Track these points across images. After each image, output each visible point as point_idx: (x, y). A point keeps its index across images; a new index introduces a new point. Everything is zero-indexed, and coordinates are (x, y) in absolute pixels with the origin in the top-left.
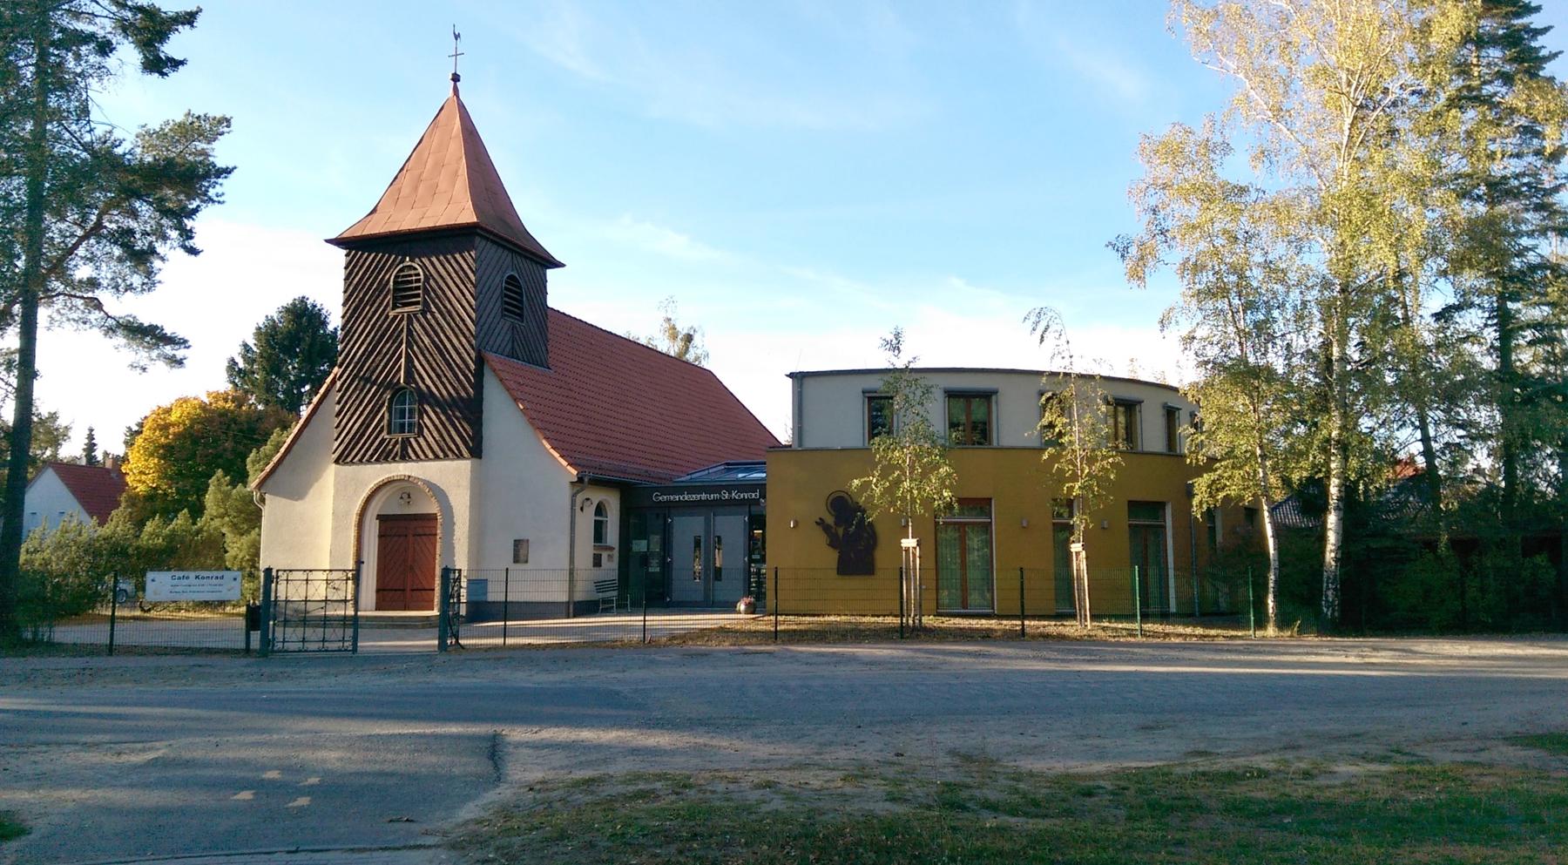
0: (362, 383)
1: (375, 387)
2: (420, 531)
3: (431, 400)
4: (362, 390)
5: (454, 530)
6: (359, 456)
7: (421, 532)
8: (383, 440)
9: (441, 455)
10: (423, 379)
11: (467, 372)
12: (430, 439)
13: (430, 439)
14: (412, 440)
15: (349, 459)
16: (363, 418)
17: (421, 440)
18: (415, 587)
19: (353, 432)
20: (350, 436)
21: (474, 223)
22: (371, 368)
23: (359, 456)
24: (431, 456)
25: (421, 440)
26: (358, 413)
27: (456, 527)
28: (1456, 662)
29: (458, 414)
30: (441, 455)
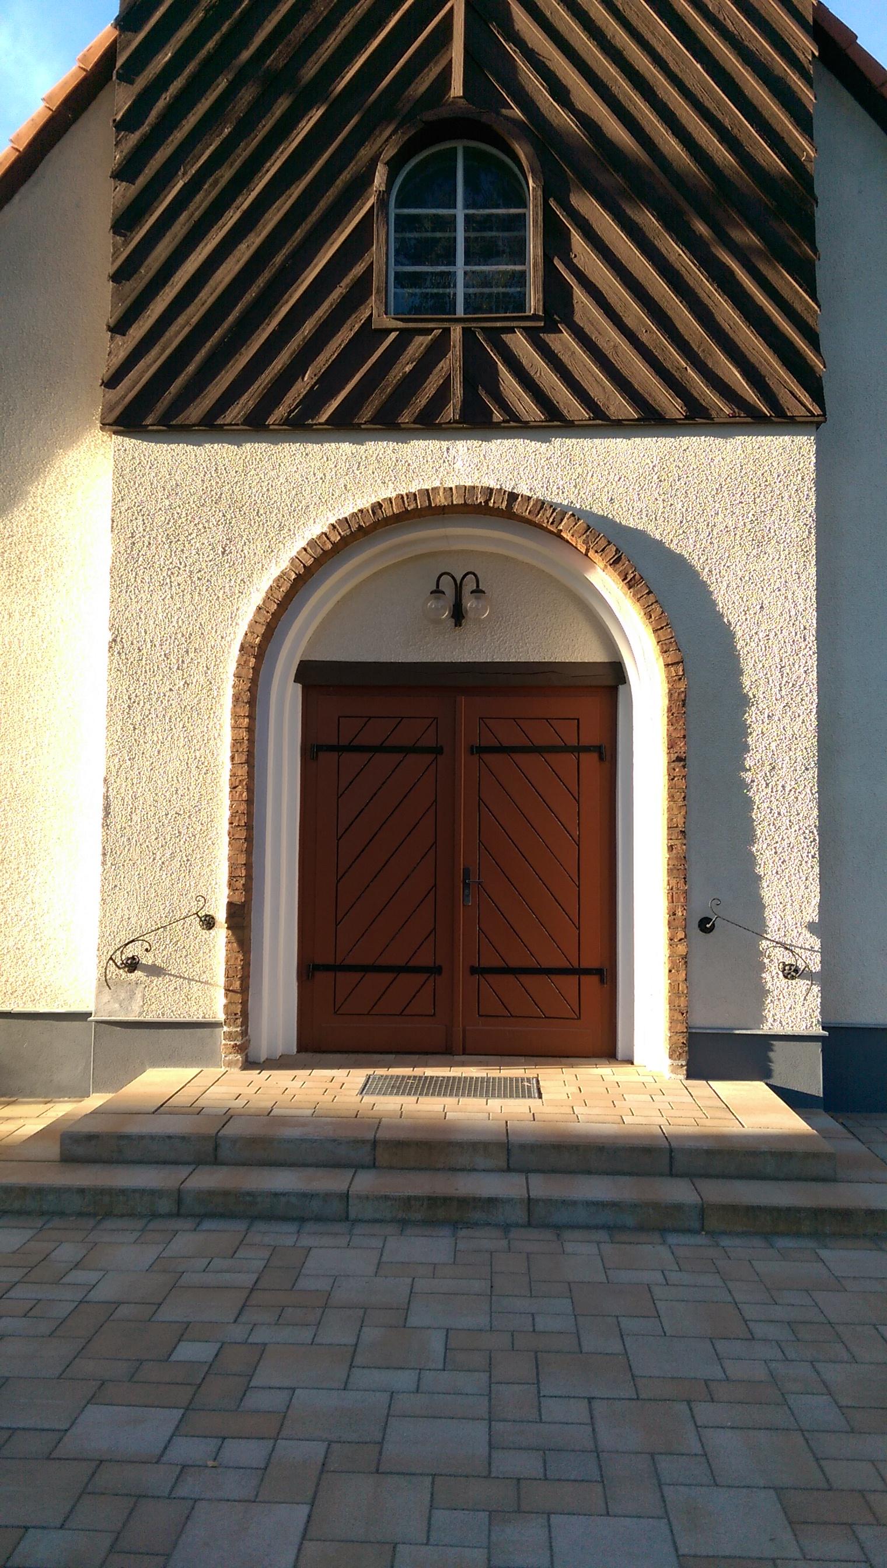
0: (247, 95)
1: (317, 114)
2: (510, 737)
3: (613, 180)
4: (244, 128)
5: (743, 731)
6: (247, 401)
7: (515, 739)
8: (369, 335)
9: (673, 407)
10: (560, 93)
11: (780, 64)
12: (609, 337)
13: (609, 337)
14: (520, 344)
15: (196, 412)
16: (254, 241)
17: (564, 342)
18: (490, 960)
19: (207, 296)
20: (194, 313)
21: (85, 76)
22: (297, 35)
23: (247, 401)
24: (620, 406)
25: (564, 342)
26: (231, 218)
27: (752, 716)
28: (329, 1119)
29: (748, 238)
30: (673, 407)
